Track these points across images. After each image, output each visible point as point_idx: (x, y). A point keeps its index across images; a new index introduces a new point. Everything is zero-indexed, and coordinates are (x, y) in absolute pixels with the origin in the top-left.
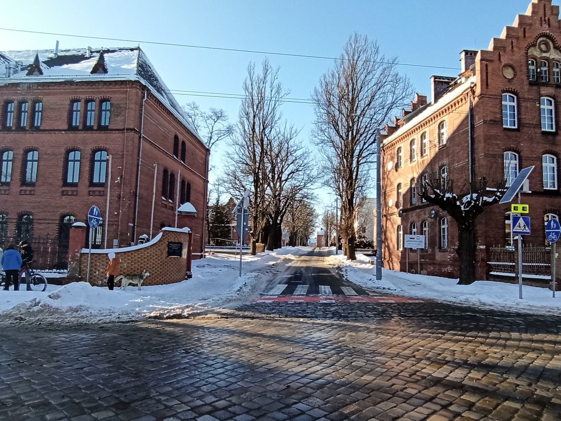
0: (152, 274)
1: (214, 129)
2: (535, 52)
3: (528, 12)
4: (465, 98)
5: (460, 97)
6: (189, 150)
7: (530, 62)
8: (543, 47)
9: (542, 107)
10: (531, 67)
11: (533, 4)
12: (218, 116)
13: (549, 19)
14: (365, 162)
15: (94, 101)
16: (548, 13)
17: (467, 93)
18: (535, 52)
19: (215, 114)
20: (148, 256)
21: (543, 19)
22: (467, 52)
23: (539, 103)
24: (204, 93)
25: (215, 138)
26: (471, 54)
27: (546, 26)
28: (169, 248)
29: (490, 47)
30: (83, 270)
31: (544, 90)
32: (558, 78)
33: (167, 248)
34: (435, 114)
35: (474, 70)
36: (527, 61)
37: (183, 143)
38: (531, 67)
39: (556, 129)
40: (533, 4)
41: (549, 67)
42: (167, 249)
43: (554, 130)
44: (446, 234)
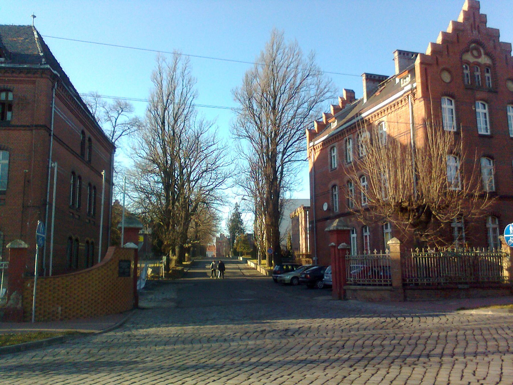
0: (104, 299)
1: (118, 122)
2: (469, 57)
3: (461, 19)
4: (405, 100)
5: (400, 99)
6: (93, 146)
7: (464, 66)
8: (475, 53)
9: (477, 110)
10: (466, 72)
11: (464, 11)
12: (122, 107)
13: (478, 26)
14: (289, 161)
15: (12, 91)
16: (477, 20)
17: (408, 96)
18: (469, 57)
19: (119, 104)
20: (99, 278)
21: (473, 26)
22: (400, 52)
23: (475, 107)
24: (108, 80)
25: (118, 133)
26: (404, 54)
27: (475, 32)
28: (120, 268)
29: (428, 52)
30: (26, 298)
31: (478, 95)
32: (489, 83)
33: (118, 267)
34: (373, 114)
35: (412, 71)
36: (462, 66)
37: (90, 140)
38: (466, 72)
39: (491, 132)
40: (464, 11)
41: (481, 72)
42: (117, 269)
43: (489, 133)
44: (368, 241)
